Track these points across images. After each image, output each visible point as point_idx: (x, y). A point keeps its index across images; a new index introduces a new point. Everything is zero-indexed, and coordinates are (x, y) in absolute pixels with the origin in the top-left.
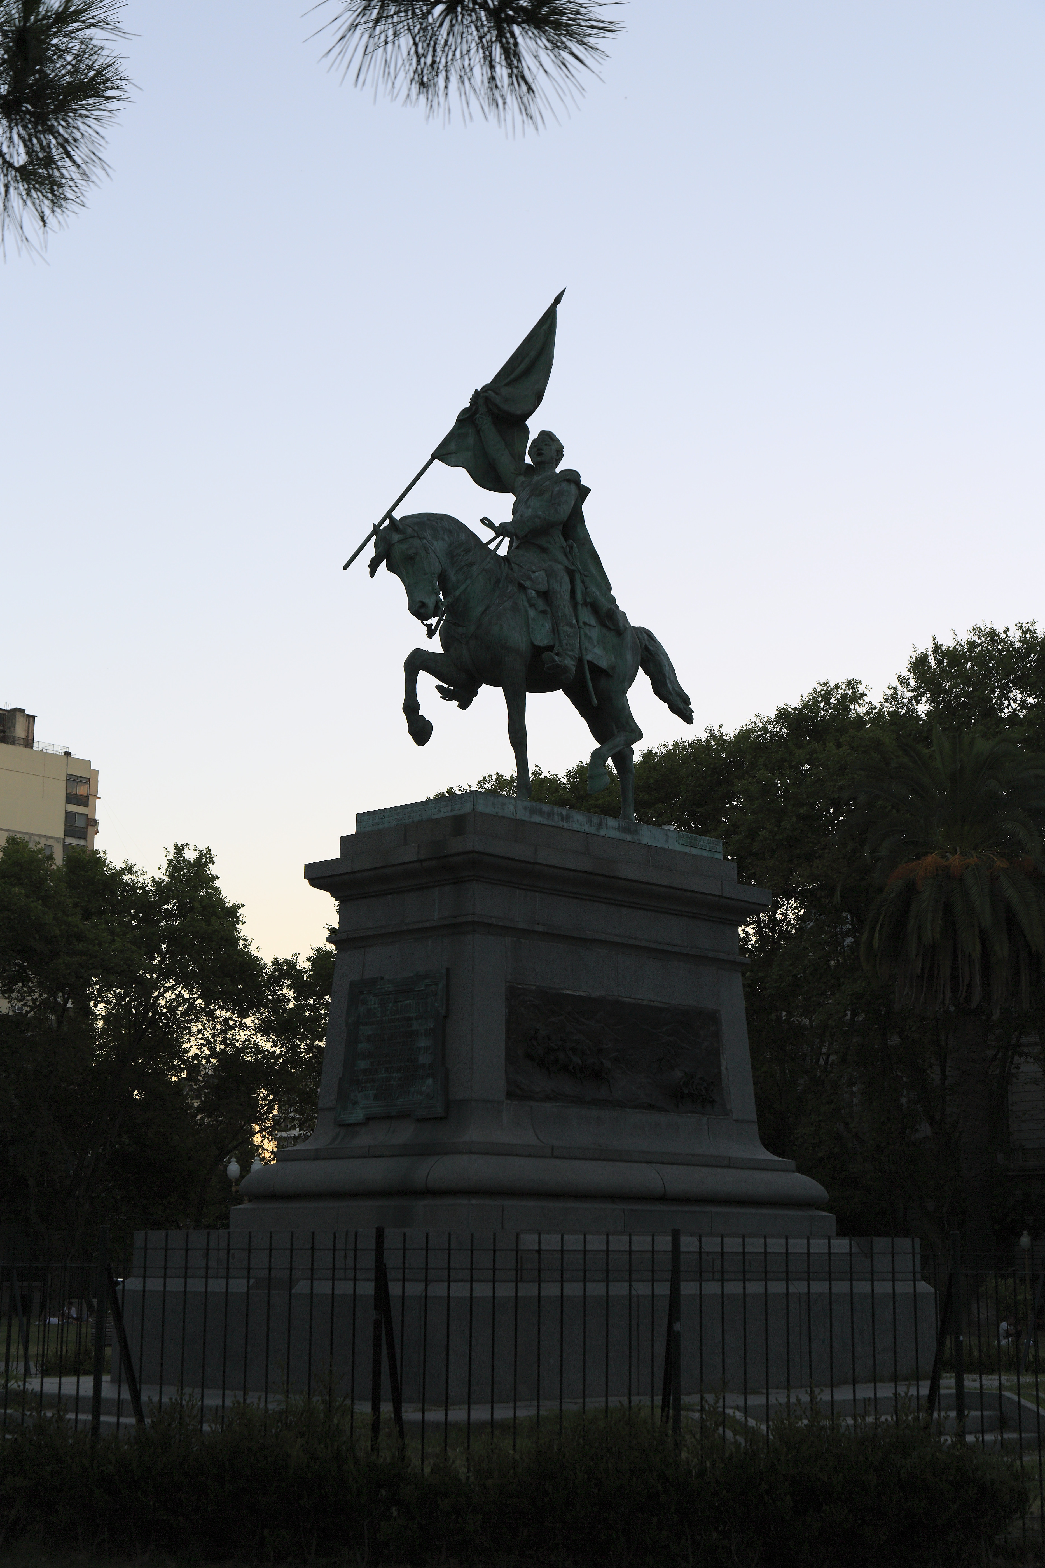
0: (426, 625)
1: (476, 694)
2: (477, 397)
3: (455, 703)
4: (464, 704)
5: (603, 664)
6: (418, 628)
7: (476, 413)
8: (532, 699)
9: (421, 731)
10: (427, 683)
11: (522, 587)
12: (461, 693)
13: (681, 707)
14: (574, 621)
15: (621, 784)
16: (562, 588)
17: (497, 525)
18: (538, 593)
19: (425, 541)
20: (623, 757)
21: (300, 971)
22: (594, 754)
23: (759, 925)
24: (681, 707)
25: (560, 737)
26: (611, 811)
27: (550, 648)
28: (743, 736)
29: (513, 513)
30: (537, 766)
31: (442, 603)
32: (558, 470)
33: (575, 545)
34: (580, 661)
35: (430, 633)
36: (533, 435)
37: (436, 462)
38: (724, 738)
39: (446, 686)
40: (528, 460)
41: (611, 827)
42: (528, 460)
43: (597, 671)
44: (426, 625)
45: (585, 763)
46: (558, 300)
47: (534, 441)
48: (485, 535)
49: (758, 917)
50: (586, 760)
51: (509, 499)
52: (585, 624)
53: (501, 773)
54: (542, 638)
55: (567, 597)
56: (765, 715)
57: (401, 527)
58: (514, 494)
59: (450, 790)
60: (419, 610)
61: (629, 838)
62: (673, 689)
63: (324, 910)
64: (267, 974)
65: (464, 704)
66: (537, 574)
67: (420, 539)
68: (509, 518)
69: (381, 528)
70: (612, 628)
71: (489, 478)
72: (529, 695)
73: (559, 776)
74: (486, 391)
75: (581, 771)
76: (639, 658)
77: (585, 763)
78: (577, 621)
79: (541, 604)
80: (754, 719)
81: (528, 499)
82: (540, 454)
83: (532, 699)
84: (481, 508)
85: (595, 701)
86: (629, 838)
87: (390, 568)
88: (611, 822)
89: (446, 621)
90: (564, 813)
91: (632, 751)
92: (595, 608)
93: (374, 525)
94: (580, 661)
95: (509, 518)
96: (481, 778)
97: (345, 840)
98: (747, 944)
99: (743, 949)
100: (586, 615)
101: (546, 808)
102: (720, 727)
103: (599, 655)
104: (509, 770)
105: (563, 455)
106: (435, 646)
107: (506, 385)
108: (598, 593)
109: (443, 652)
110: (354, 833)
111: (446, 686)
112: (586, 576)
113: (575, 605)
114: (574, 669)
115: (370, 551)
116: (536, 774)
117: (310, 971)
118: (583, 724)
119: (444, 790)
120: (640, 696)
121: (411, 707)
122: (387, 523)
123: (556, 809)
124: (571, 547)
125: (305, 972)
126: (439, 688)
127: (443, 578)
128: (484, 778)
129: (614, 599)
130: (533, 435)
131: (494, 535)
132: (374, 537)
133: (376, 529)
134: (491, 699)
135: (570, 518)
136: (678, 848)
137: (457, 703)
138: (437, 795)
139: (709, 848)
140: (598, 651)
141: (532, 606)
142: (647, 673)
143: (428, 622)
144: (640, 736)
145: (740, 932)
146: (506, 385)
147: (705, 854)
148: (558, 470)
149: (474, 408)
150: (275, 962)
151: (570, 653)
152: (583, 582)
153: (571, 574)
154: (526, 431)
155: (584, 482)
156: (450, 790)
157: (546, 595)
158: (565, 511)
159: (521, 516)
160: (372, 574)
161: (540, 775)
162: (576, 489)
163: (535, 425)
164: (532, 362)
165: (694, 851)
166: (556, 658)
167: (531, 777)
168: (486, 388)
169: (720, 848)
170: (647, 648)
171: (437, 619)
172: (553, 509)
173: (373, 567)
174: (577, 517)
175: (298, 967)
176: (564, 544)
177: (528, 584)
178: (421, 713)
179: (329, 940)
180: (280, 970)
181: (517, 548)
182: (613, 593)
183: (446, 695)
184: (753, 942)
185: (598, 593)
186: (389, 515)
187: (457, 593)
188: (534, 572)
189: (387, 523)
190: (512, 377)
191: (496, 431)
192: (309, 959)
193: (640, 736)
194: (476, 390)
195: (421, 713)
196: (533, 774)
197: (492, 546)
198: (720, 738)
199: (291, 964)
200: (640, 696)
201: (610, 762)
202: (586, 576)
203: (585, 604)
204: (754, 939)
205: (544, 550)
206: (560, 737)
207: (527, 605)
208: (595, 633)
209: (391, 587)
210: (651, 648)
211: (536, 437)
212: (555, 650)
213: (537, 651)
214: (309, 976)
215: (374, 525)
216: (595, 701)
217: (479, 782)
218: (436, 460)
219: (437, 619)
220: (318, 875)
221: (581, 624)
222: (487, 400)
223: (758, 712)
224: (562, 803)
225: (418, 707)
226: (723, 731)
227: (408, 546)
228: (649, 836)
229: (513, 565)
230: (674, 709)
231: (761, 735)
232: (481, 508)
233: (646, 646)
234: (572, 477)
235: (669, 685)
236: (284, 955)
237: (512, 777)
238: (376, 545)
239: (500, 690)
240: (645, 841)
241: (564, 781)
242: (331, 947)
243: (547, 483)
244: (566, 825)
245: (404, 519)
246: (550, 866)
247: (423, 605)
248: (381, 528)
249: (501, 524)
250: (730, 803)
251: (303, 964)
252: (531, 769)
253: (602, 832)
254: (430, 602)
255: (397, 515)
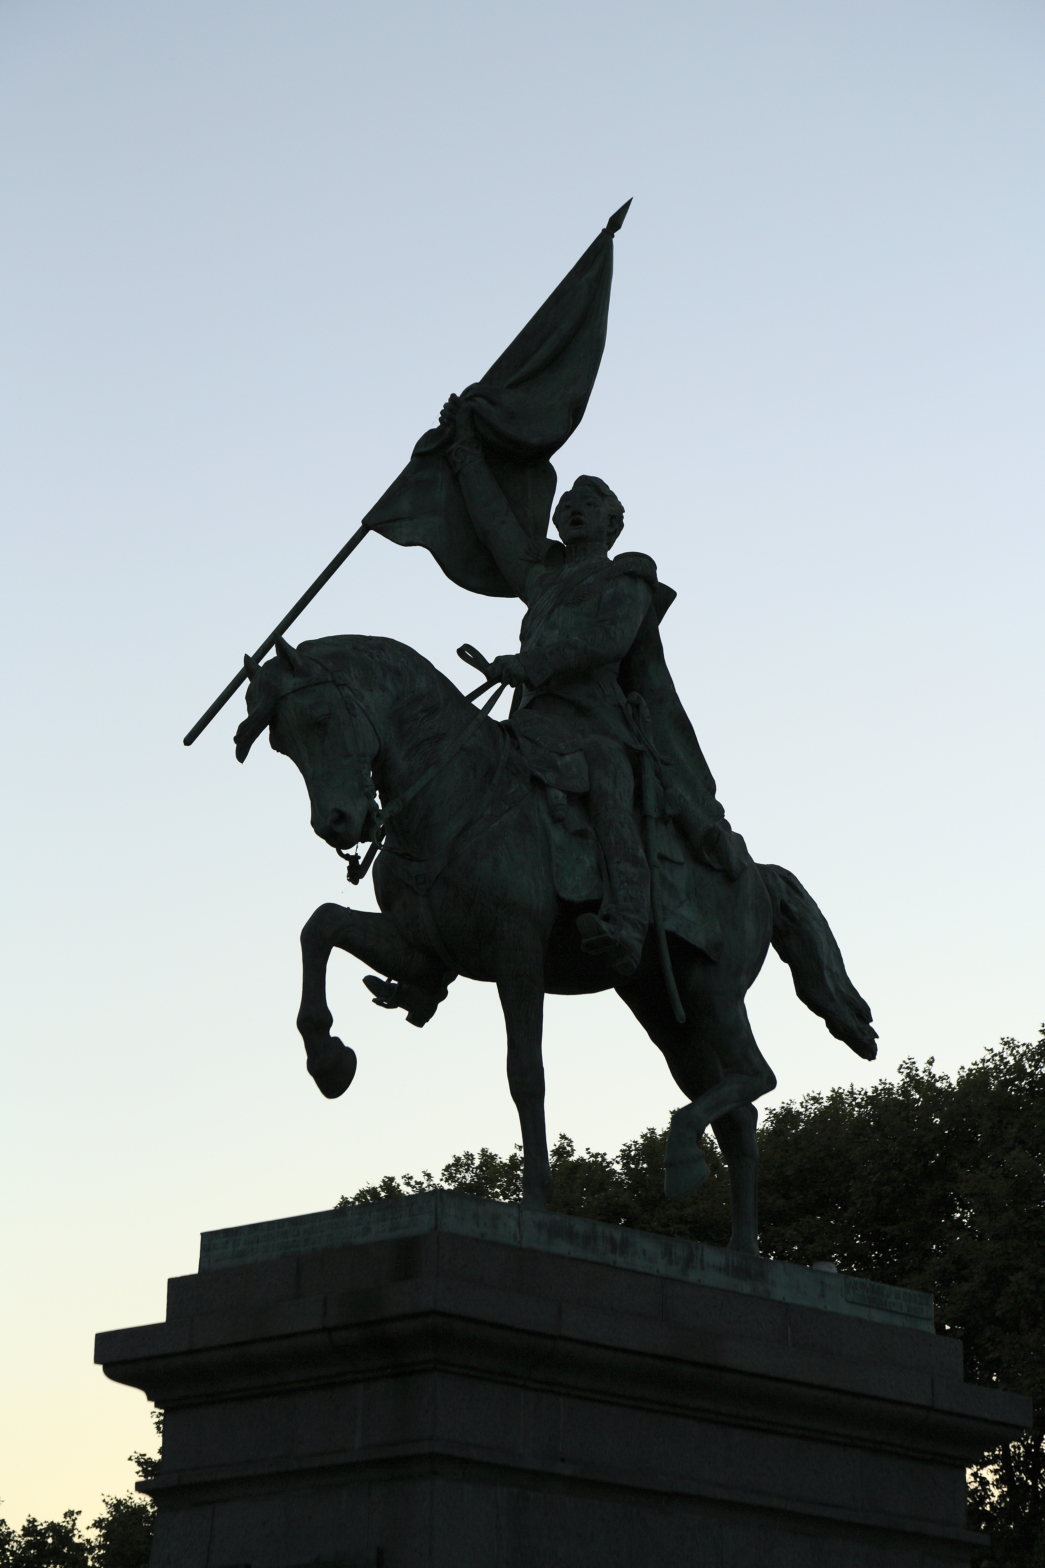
0: (347, 857)
1: (443, 995)
2: (454, 409)
3: (401, 1013)
4: (420, 1016)
5: (698, 938)
6: (329, 863)
7: (449, 441)
8: (554, 1005)
9: (332, 1068)
10: (346, 971)
11: (537, 783)
12: (414, 993)
13: (852, 1024)
14: (641, 853)
15: (727, 1166)
16: (619, 788)
17: (490, 660)
18: (571, 796)
19: (347, 691)
20: (736, 1122)
21: (80, 1548)
22: (678, 1116)
23: (1006, 1466)
24: (852, 1024)
25: (611, 1081)
26: (711, 1231)
27: (592, 906)
28: (976, 1081)
29: (522, 638)
30: (563, 1137)
31: (379, 814)
32: (612, 555)
33: (645, 704)
34: (652, 932)
35: (355, 874)
36: (564, 485)
37: (372, 536)
38: (938, 1085)
39: (384, 978)
40: (553, 533)
41: (711, 1266)
42: (553, 533)
43: (684, 952)
44: (347, 857)
45: (659, 1132)
46: (616, 222)
47: (566, 496)
48: (466, 679)
49: (1006, 1450)
50: (662, 1125)
51: (514, 610)
52: (662, 858)
53: (492, 1150)
54: (577, 885)
55: (627, 803)
56: (1020, 1039)
57: (300, 662)
58: (524, 600)
59: (388, 1183)
60: (332, 827)
61: (746, 1288)
62: (838, 990)
63: (133, 1424)
64: (13, 1553)
65: (420, 1016)
66: (568, 758)
67: (338, 686)
68: (513, 647)
69: (261, 664)
70: (717, 866)
71: (475, 567)
72: (546, 995)
73: (609, 1158)
74: (470, 399)
75: (651, 1146)
76: (770, 928)
77: (659, 1132)
78: (647, 851)
79: (575, 818)
80: (998, 1048)
81: (552, 611)
82: (577, 523)
83: (554, 1005)
84: (457, 627)
85: (681, 1013)
86: (746, 1288)
87: (277, 744)
88: (712, 1255)
89: (385, 849)
90: (618, 1235)
91: (754, 1112)
92: (682, 828)
93: (246, 656)
94: (652, 932)
95: (513, 647)
96: (451, 1161)
97: (176, 1286)
98: (982, 1502)
99: (975, 1513)
100: (664, 841)
101: (580, 1225)
102: (931, 1062)
103: (688, 920)
104: (506, 1141)
105: (621, 526)
106: (363, 898)
107: (510, 387)
108: (688, 798)
109: (377, 909)
110: (195, 1270)
111: (384, 978)
112: (667, 764)
113: (643, 821)
114: (639, 947)
115: (237, 710)
116: (562, 1152)
117: (100, 1547)
118: (656, 1058)
119: (377, 1183)
120: (771, 1001)
121: (314, 1019)
122: (272, 654)
123: (600, 1228)
124: (637, 707)
125: (91, 1550)
126: (370, 982)
127: (381, 764)
128: (458, 1160)
129: (720, 810)
130: (564, 485)
131: (482, 679)
132: (247, 682)
133: (250, 665)
134: (473, 1005)
135: (634, 647)
136: (845, 1309)
137: (406, 1013)
138: (362, 1194)
139: (909, 1311)
140: (688, 912)
141: (558, 821)
142: (784, 958)
143: (351, 852)
144: (768, 1082)
145: (969, 1478)
146: (510, 387)
147: (899, 1321)
148: (612, 555)
149: (448, 430)
150: (30, 1529)
151: (632, 916)
152: (658, 775)
153: (636, 759)
154: (551, 477)
155: (663, 577)
156: (388, 1183)
157: (583, 800)
158: (624, 635)
159: (538, 644)
160: (242, 755)
161: (570, 1154)
162: (644, 591)
163: (569, 465)
164: (563, 344)
165: (878, 1316)
166: (604, 926)
167: (552, 1160)
168: (472, 391)
169: (930, 1308)
170: (784, 908)
171: (368, 844)
172: (600, 620)
173: (244, 742)
174: (650, 647)
175: (76, 1540)
176: (623, 700)
177: (549, 777)
178: (333, 1032)
179: (140, 1487)
180: (40, 1545)
181: (529, 706)
182: (718, 797)
183: (385, 996)
184: (994, 1499)
185: (688, 798)
186: (276, 638)
187: (410, 794)
188: (563, 755)
189: (272, 654)
190: (525, 369)
191: (492, 472)
192: (98, 1524)
193: (768, 1082)
194: (453, 395)
195: (333, 1032)
196: (556, 1152)
197: (479, 703)
198: (931, 1085)
199: (61, 1534)
200: (771, 1001)
201: (709, 1130)
202: (667, 764)
203: (664, 819)
204: (997, 1492)
205: (582, 711)
206: (611, 1081)
207: (548, 820)
208: (682, 876)
209: (277, 780)
210: (793, 908)
211: (569, 488)
212: (603, 910)
213: (568, 911)
214: (98, 1559)
215: (246, 656)
216: (681, 1013)
217: (448, 1168)
218: (372, 534)
219: (368, 844)
220: (122, 1355)
221: (655, 858)
222: (473, 413)
223: (1008, 1034)
224: (610, 1215)
225: (327, 1020)
226: (937, 1071)
227: (316, 702)
228: (787, 1284)
229: (521, 740)
230: (837, 1030)
231: (1011, 1082)
232: (457, 627)
233: (782, 902)
234: (640, 567)
235: (829, 983)
236: (49, 1514)
237: (513, 1158)
238: (249, 697)
239: (490, 989)
240: (780, 1294)
241: (618, 1167)
242: (142, 1499)
243: (591, 579)
244: (620, 1261)
245: (306, 646)
246: (588, 1344)
247: (342, 817)
248: (261, 664)
249: (498, 659)
250: (949, 1218)
251: (86, 1532)
252: (552, 1142)
253: (693, 1276)
254: (356, 812)
255: (294, 637)
